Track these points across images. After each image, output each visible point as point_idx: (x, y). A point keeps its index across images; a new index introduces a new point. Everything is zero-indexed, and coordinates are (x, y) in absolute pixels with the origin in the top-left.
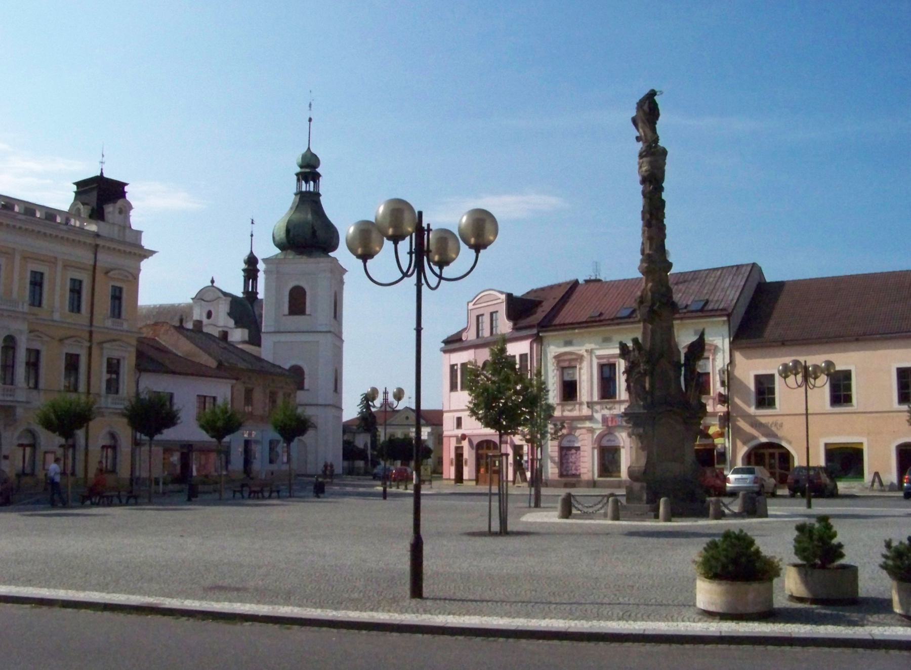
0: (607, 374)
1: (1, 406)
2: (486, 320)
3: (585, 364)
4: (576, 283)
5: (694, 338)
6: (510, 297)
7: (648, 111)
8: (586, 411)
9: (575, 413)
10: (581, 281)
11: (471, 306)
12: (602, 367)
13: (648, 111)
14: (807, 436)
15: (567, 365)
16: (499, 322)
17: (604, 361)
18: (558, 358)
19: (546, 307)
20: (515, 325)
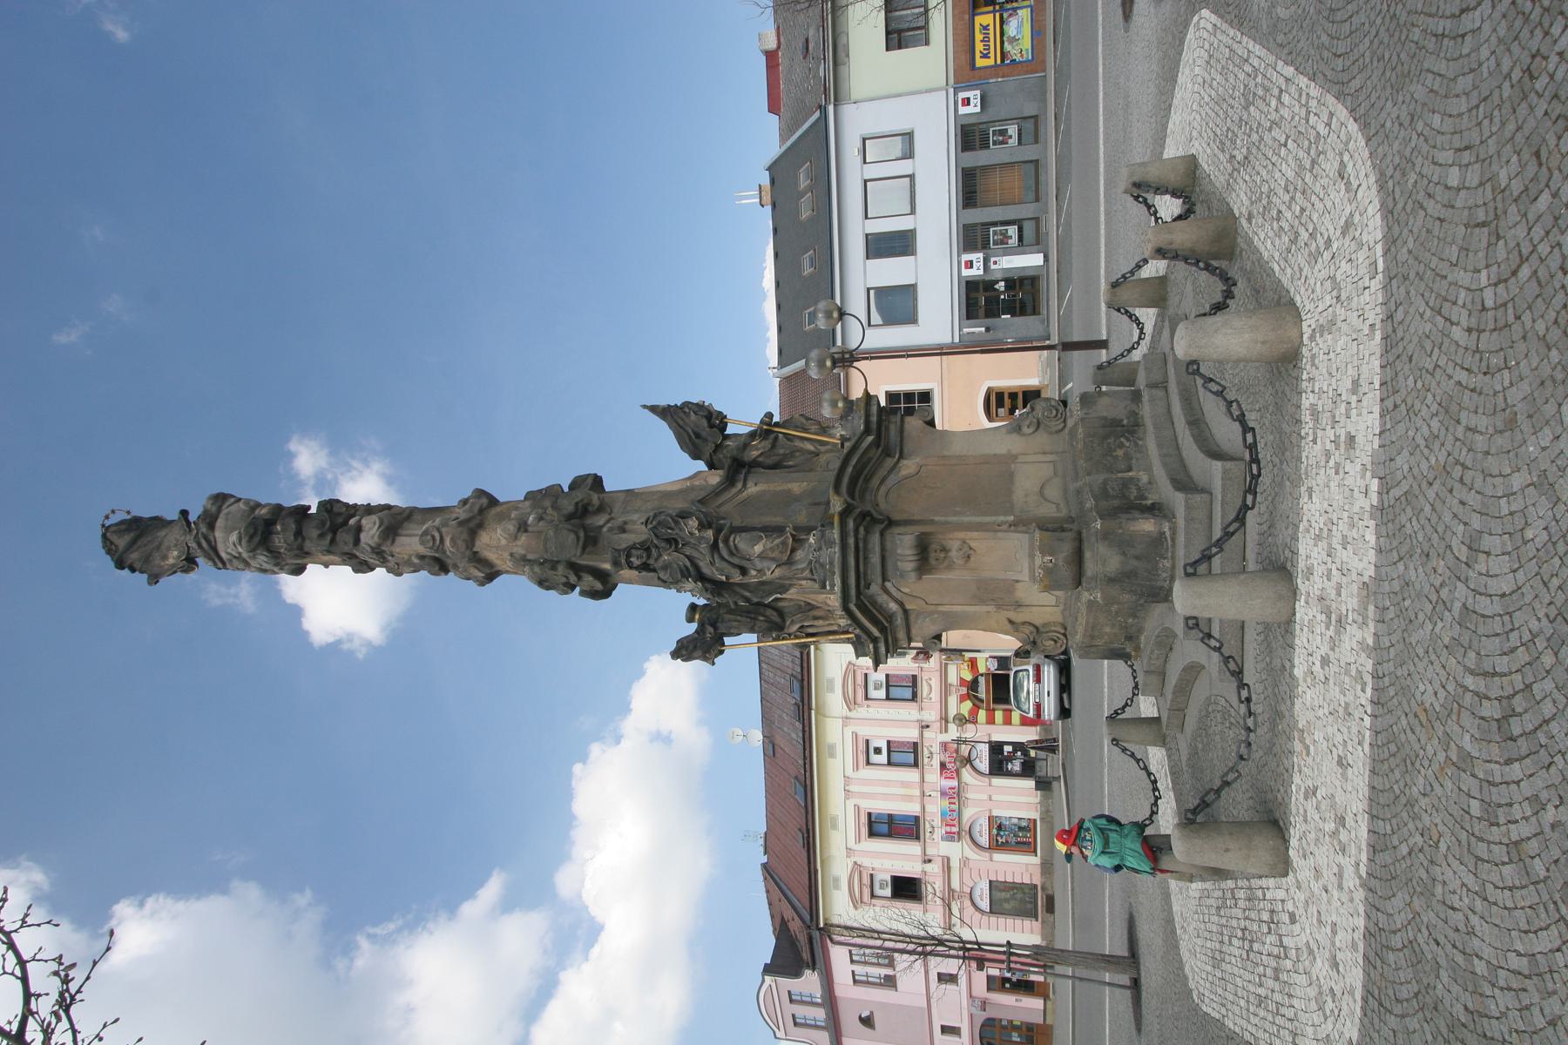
0: (884, 828)
1: (1044, 2)
2: (801, 1011)
3: (866, 862)
4: (764, 866)
5: (663, 433)
6: (768, 970)
7: (134, 543)
8: (934, 868)
9: (938, 885)
10: (765, 859)
11: (780, 1034)
12: (872, 834)
13: (134, 543)
14: (899, 95)
15: (865, 889)
16: (806, 991)
17: (865, 830)
18: (857, 902)
19: (789, 914)
20: (808, 967)
